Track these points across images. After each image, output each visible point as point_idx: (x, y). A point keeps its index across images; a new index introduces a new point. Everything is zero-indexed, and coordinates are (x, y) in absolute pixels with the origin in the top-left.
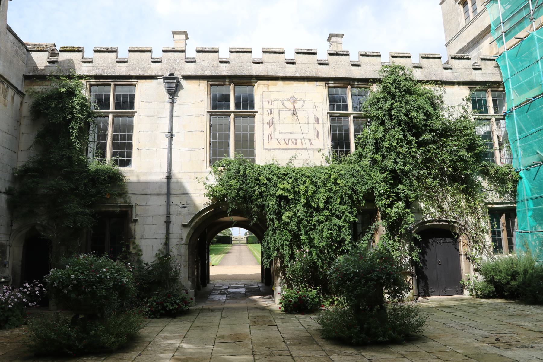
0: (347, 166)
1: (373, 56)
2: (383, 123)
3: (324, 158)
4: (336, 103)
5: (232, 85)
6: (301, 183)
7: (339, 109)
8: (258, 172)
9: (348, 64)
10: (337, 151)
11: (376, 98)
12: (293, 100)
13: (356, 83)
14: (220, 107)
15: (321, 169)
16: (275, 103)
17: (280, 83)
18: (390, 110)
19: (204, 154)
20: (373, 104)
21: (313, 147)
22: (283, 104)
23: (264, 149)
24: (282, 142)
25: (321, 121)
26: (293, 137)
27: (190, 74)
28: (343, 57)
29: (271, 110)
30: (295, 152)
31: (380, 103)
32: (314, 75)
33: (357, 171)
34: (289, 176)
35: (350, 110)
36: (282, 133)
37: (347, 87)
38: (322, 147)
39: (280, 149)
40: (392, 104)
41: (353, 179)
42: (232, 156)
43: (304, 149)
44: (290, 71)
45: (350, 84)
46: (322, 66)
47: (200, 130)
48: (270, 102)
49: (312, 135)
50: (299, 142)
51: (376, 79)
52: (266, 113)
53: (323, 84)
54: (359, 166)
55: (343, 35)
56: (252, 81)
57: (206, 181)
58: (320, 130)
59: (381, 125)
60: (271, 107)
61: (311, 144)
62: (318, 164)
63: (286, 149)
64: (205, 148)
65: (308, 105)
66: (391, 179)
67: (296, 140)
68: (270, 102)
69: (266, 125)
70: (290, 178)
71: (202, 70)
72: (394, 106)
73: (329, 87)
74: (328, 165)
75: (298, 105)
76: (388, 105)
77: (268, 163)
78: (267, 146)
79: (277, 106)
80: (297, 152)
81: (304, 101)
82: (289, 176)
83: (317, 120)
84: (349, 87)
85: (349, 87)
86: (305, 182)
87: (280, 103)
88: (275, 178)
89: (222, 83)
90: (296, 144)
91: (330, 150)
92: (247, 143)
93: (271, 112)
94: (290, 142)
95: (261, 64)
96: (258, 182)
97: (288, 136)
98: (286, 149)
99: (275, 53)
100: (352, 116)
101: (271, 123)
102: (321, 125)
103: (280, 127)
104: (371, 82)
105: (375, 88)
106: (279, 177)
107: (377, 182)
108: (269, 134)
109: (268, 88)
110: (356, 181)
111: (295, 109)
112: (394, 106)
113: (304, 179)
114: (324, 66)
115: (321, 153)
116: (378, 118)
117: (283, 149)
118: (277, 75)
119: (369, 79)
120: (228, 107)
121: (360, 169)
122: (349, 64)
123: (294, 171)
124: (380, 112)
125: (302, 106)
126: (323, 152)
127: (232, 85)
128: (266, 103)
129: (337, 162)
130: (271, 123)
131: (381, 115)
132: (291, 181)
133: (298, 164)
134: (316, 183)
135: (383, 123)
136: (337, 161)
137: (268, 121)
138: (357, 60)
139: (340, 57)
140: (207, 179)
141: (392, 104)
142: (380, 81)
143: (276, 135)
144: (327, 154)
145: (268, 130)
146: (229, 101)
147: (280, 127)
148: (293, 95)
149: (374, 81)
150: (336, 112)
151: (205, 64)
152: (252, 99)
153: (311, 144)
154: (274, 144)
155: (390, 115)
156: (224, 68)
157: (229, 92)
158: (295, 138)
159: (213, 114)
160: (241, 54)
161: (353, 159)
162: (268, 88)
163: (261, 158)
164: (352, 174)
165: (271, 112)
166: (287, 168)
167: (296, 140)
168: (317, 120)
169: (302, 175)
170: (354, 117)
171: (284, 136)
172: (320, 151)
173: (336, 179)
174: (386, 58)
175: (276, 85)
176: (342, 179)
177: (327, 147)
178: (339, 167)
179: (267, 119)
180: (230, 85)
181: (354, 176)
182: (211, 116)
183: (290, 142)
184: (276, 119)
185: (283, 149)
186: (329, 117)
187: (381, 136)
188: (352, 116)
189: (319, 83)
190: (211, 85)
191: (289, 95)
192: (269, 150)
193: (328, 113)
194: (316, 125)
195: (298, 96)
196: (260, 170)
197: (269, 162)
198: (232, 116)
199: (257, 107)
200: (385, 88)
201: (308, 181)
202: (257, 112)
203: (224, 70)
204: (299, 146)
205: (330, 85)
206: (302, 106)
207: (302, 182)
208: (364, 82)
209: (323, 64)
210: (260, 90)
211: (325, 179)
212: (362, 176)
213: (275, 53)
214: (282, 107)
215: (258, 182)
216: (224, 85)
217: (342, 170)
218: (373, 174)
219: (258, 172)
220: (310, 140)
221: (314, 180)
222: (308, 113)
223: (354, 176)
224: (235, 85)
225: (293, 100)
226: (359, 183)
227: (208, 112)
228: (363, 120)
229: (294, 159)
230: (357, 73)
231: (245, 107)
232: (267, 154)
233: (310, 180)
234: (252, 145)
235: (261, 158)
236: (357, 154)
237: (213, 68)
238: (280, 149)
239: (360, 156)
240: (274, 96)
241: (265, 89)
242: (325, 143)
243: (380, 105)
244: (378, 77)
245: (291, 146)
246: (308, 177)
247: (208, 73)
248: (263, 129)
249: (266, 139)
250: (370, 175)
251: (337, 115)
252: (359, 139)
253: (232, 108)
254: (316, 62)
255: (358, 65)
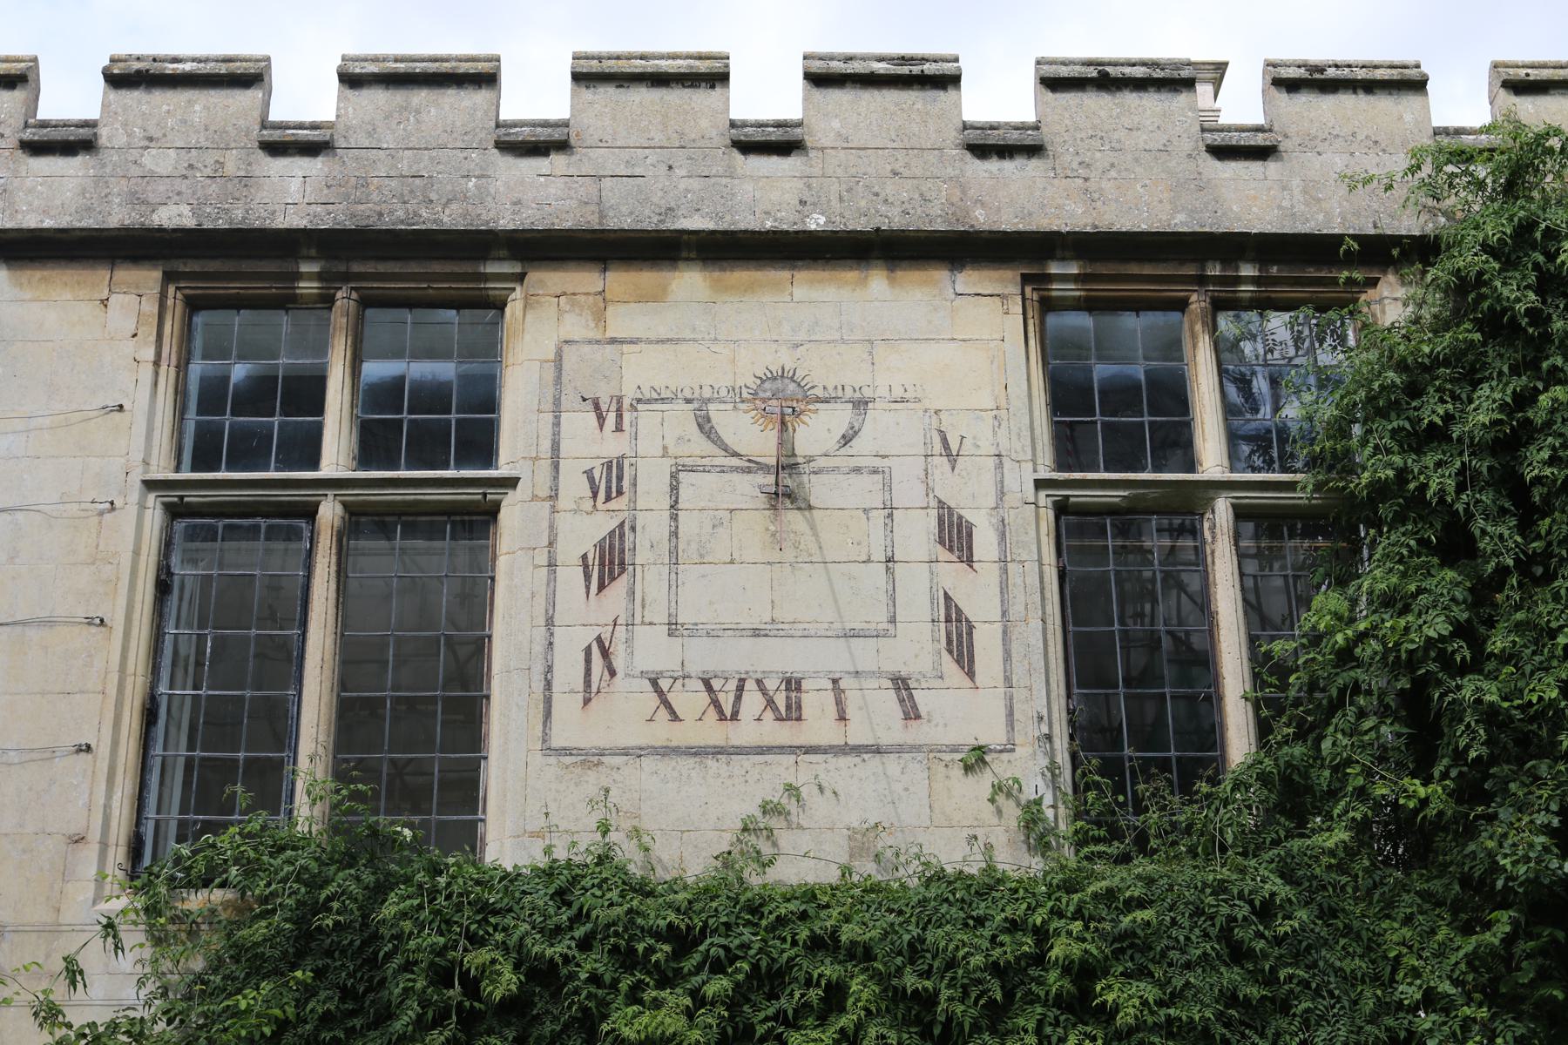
0: (1185, 872)
1: (1369, 87)
2: (1455, 544)
3: (1012, 812)
4: (1104, 419)
5: (344, 299)
6: (804, 1008)
7: (1124, 454)
8: (467, 918)
9: (1187, 145)
10: (1111, 768)
11: (1402, 366)
12: (783, 401)
13: (1247, 270)
14: (248, 451)
15: (971, 895)
16: (648, 419)
17: (689, 281)
18: (1510, 440)
19: (95, 796)
20: (1379, 406)
21: (918, 733)
22: (705, 426)
23: (548, 750)
24: (690, 700)
25: (985, 543)
26: (776, 658)
27: (48, 223)
28: (1151, 102)
29: (615, 468)
30: (784, 769)
31: (1432, 396)
32: (934, 217)
33: (1266, 910)
34: (712, 945)
35: (1212, 458)
36: (693, 631)
37: (1181, 305)
38: (993, 735)
39: (667, 751)
40: (1525, 399)
41: (1231, 976)
42: (307, 813)
43: (858, 750)
44: (768, 197)
45: (1202, 280)
46: (993, 165)
47: (81, 613)
48: (609, 412)
49: (916, 646)
50: (816, 702)
51: (1396, 240)
52: (573, 486)
53: (1003, 280)
54: (1287, 875)
55: (1221, 67)
56: (491, 268)
57: (60, 993)
58: (980, 604)
59: (1446, 562)
60: (613, 446)
61: (912, 713)
62: (954, 855)
63: (718, 751)
64: (103, 750)
65: (889, 432)
66: (1543, 977)
67: (793, 684)
68: (609, 412)
69: (570, 576)
70: (718, 968)
71: (135, 199)
72: (1538, 415)
73: (1048, 305)
74: (1037, 865)
75: (816, 433)
76: (1484, 409)
77: (561, 854)
78: (571, 726)
79: (658, 437)
80: (804, 772)
81: (861, 404)
82: (712, 945)
83: (955, 536)
84: (1198, 302)
85: (1198, 302)
86: (835, 996)
87: (681, 420)
88: (595, 962)
89: (273, 289)
90: (793, 713)
91: (1063, 758)
92: (422, 721)
93: (611, 481)
94: (753, 701)
95: (557, 161)
96: (455, 992)
97: (734, 657)
98: (718, 751)
99: (660, 80)
100: (1222, 509)
101: (609, 563)
102: (988, 573)
103: (674, 586)
104: (1351, 260)
105: (1392, 303)
106: (626, 958)
107: (1430, 1000)
108: (589, 636)
109: (600, 317)
110: (1254, 992)
111: (787, 464)
112: (1538, 415)
113: (829, 970)
114: (1009, 166)
115: (982, 784)
116: (1416, 505)
117: (698, 752)
118: (671, 225)
119: (1338, 239)
120: (310, 452)
121: (1284, 891)
122: (1189, 142)
123: (755, 909)
124: (1430, 460)
125: (846, 440)
126: (1001, 768)
127: (344, 299)
128: (579, 423)
129: (1115, 848)
130: (609, 563)
131: (1440, 481)
132: (717, 986)
133: (804, 862)
134: (928, 1000)
135: (1455, 544)
136: (1115, 834)
137: (588, 546)
138: (1260, 120)
139: (1130, 98)
140: (73, 973)
141: (1525, 399)
142: (1416, 252)
143: (650, 650)
144: (1035, 785)
145: (583, 614)
146: (319, 409)
147: (674, 586)
148: (784, 359)
149: (1381, 253)
150: (1104, 485)
151: (162, 162)
152: (483, 399)
153: (912, 713)
154: (625, 715)
155: (1513, 487)
156: (295, 185)
157: (322, 349)
158: (794, 667)
159: (193, 497)
160: (420, 96)
161: (1240, 815)
162: (600, 317)
163: (524, 817)
164: (1226, 934)
165: (611, 481)
166: (707, 893)
167: (793, 684)
168: (955, 536)
169: (817, 944)
170: (1241, 514)
171: (702, 656)
172: (977, 759)
173: (1084, 973)
174: (1462, 103)
175: (656, 297)
176: (1142, 973)
177: (1028, 732)
178: (1109, 877)
179: (584, 531)
180: (327, 301)
181: (1238, 954)
182: (174, 512)
183: (753, 701)
184: (652, 527)
185: (698, 752)
186: (1048, 516)
187: (1438, 626)
188: (1222, 509)
189: (970, 280)
190: (194, 305)
191: (751, 363)
192: (591, 758)
193: (1040, 484)
194: (952, 575)
195: (820, 371)
196: (488, 904)
197: (575, 840)
198: (330, 512)
199: (510, 456)
200: (1464, 288)
201: (861, 989)
202: (511, 483)
203: (291, 196)
204: (818, 725)
205: (1058, 289)
206: (846, 440)
207: (814, 994)
208: (1312, 268)
209: (1005, 151)
210: (544, 336)
211: (995, 969)
212: (1299, 949)
213: (660, 80)
214: (700, 445)
215: (455, 992)
216: (286, 302)
217: (1142, 904)
218: (1395, 934)
219: (467, 918)
220: (901, 684)
221: (910, 981)
222: (888, 487)
223: (1238, 954)
224: (367, 302)
225: (783, 401)
226: (1284, 1007)
227: (150, 485)
228: (1307, 533)
229: (775, 822)
230: (1250, 202)
231: (428, 448)
232: (571, 778)
233: (877, 977)
234: (466, 718)
235: (524, 817)
236: (1264, 778)
237: (214, 188)
238: (667, 751)
239: (1293, 797)
240: (640, 371)
241: (576, 325)
242: (1014, 703)
243: (1432, 410)
244: (1409, 224)
245: (754, 727)
246: (861, 954)
247: (174, 215)
248: (551, 602)
249: (568, 672)
250: (1371, 947)
251: (1115, 496)
252: (1282, 671)
253: (337, 454)
254: (953, 135)
255: (1263, 153)
